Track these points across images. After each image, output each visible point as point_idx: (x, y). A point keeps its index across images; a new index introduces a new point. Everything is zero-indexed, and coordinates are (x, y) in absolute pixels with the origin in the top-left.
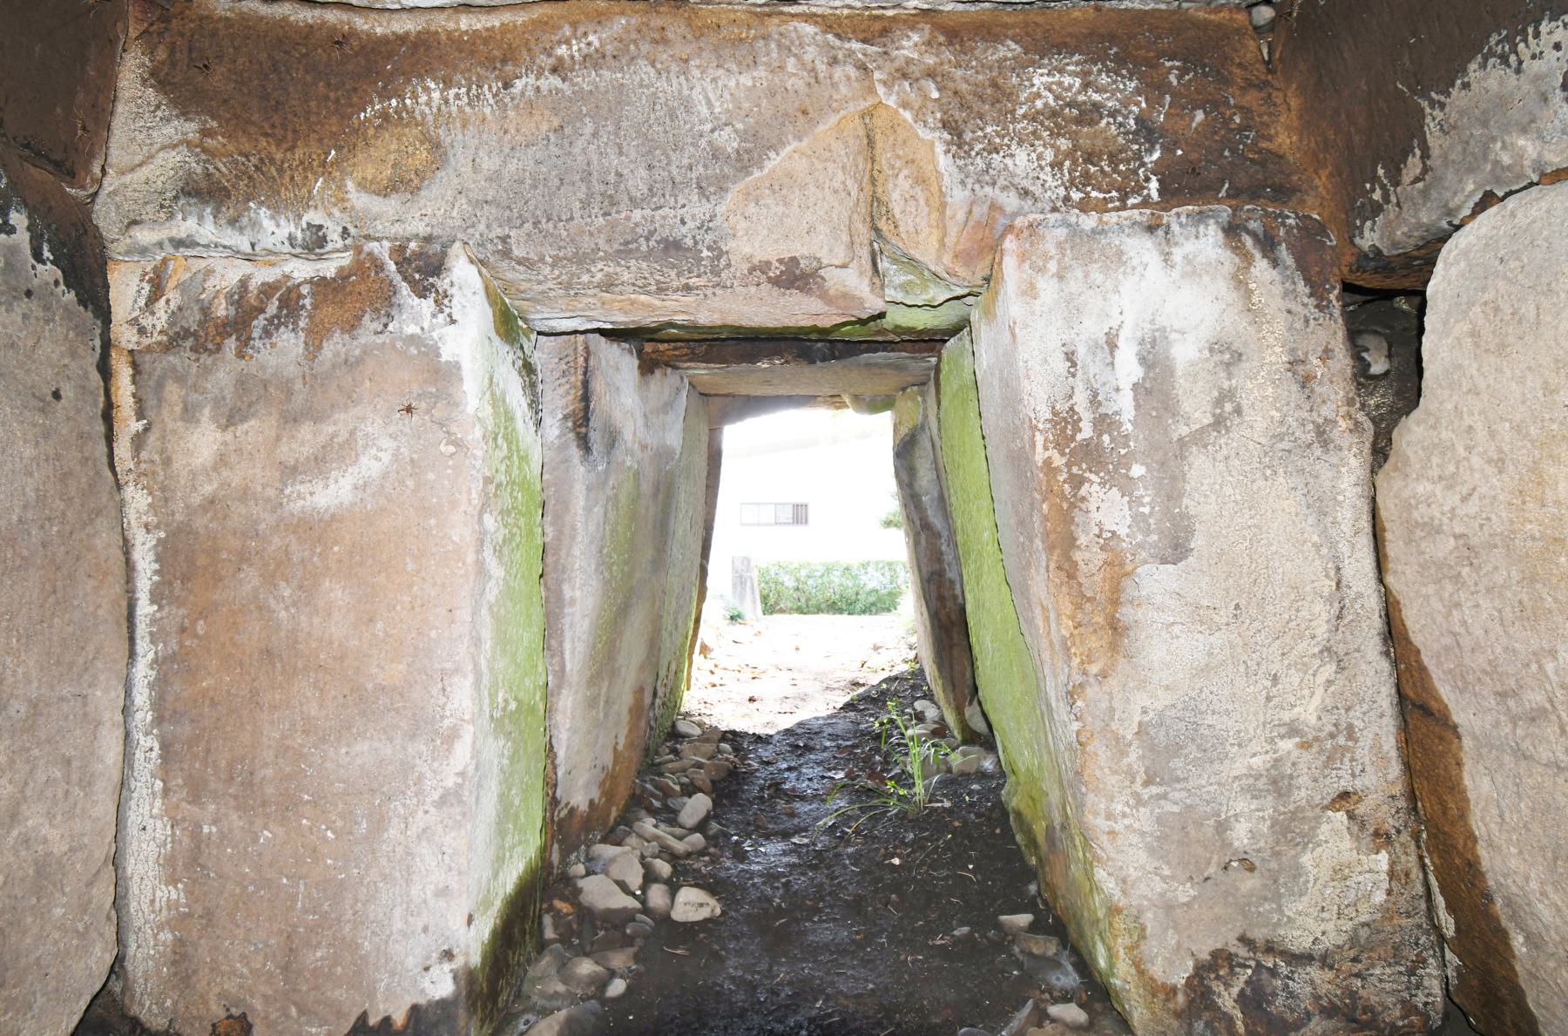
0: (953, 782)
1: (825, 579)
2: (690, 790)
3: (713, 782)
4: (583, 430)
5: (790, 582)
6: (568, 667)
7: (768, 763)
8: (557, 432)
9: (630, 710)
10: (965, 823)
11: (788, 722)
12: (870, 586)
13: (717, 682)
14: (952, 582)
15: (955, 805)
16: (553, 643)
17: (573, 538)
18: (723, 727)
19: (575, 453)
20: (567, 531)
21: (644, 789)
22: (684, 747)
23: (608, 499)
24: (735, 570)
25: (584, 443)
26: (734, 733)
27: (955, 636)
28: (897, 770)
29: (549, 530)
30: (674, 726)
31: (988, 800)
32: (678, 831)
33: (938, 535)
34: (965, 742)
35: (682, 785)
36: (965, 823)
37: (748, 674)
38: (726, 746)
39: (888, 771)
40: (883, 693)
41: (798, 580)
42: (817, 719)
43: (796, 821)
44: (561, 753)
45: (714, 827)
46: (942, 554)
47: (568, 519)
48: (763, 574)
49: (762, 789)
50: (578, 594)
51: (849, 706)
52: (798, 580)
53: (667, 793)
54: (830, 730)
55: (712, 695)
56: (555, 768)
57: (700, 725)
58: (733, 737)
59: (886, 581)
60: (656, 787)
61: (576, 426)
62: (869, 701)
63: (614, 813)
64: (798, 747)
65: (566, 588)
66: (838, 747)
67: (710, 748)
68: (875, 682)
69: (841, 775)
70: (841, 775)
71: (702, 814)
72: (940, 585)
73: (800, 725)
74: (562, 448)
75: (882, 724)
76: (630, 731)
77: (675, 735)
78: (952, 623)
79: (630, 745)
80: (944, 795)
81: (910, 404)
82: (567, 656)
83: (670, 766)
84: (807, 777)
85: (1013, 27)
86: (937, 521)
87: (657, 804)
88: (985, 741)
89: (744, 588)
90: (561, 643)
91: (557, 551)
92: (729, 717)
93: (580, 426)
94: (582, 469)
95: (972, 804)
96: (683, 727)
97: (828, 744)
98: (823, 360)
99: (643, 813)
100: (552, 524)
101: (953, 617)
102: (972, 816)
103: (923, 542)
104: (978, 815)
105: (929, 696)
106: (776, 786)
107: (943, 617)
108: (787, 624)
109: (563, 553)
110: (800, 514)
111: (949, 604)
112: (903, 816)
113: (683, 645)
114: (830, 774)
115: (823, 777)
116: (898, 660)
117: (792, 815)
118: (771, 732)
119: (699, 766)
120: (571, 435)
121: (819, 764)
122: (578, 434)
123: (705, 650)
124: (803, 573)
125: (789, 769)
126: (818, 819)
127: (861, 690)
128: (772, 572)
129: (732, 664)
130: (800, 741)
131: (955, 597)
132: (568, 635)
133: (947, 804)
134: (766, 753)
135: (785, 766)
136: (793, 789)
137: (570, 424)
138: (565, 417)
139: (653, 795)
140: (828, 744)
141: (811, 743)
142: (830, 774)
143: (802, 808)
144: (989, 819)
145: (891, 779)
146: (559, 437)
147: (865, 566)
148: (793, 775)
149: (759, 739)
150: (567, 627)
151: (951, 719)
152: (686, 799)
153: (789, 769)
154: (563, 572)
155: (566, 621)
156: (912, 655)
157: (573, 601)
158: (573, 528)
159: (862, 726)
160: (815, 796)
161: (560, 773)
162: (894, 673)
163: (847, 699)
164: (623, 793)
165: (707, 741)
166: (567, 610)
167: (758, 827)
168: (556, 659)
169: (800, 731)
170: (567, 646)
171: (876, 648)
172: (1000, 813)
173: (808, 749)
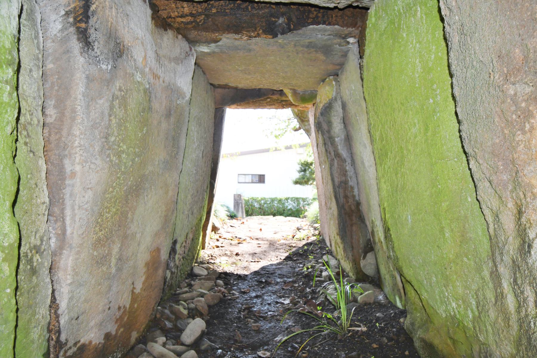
0: (363, 311)
1: (271, 204)
2: (194, 313)
3: (209, 306)
4: (83, 25)
5: (256, 205)
6: (69, 231)
7: (244, 293)
8: (60, 27)
9: (147, 264)
10: (381, 345)
11: (255, 267)
12: (289, 208)
13: (220, 245)
14: (352, 188)
15: (369, 330)
16: (56, 210)
17: (73, 119)
18: (220, 270)
19: (75, 45)
20: (67, 114)
21: (162, 313)
22: (196, 283)
23: (114, 97)
24: (235, 200)
25: (84, 37)
26: (226, 274)
27: (354, 218)
28: (321, 299)
29: (51, 111)
30: (192, 269)
31: (393, 327)
32: (179, 348)
33: (344, 161)
34: (358, 280)
35: (189, 309)
36: (381, 345)
37: (236, 242)
38: (220, 282)
39: (316, 299)
40: (305, 251)
41: (260, 205)
42: (272, 265)
43: (261, 336)
44: (63, 304)
45: (206, 343)
46: (346, 171)
47: (68, 103)
48: (247, 202)
49: (240, 312)
50: (78, 168)
51: (288, 258)
52: (260, 205)
53: (178, 316)
54: (279, 272)
55: (217, 252)
56: (57, 317)
57: (208, 269)
58: (226, 276)
59: (295, 205)
60: (172, 312)
61: (77, 21)
62: (298, 255)
63: (135, 335)
64: (262, 282)
65: (67, 162)
66: (285, 282)
67: (210, 284)
68: (301, 246)
69: (287, 301)
70: (287, 301)
71: (198, 333)
72: (345, 189)
73: (263, 268)
74: (64, 40)
75: (308, 268)
76: (147, 279)
77: (192, 275)
78: (352, 211)
79: (147, 286)
80: (361, 321)
81: (327, 88)
82: (68, 221)
83: (184, 296)
84: (268, 303)
85: (329, 30)
86: (344, 153)
87: (169, 325)
88: (376, 282)
89: (238, 207)
90: (63, 210)
91: (59, 131)
92: (224, 265)
93: (80, 21)
94: (82, 60)
95: (382, 330)
96: (197, 270)
97: (279, 280)
98: (282, 34)
99: (158, 332)
100: (55, 107)
101: (353, 208)
102: (385, 340)
103: (336, 164)
104: (390, 339)
105: (330, 253)
106: (249, 309)
107: (346, 207)
108: (255, 221)
109: (64, 132)
110: (261, 179)
111: (351, 200)
112: (333, 336)
113: (198, 225)
114: (281, 300)
115: (277, 303)
116: (310, 235)
117: (258, 331)
118: (246, 273)
119: (202, 295)
120: (72, 29)
121: (274, 293)
122: (78, 28)
123: (215, 229)
124: (262, 202)
125: (257, 297)
126: (275, 335)
127: (294, 249)
128: (250, 201)
129: (228, 236)
130: (263, 278)
131: (354, 196)
132: (68, 203)
133: (365, 329)
134: (243, 286)
135: (254, 294)
136: (259, 312)
137: (71, 20)
138: (67, 14)
139: (168, 319)
140: (279, 280)
141: (269, 280)
142: (281, 300)
143: (265, 325)
144: (397, 342)
145: (319, 305)
146: (62, 30)
147: (287, 199)
148: (259, 301)
149: (239, 277)
150: (67, 197)
151: (347, 266)
152: (191, 320)
153: (257, 297)
154: (64, 149)
155: (67, 191)
156: (317, 232)
157: (73, 174)
158: (74, 111)
159: (297, 270)
160: (273, 316)
161: (62, 321)
162: (309, 241)
163: (287, 254)
164: (143, 321)
165: (209, 279)
166: (67, 182)
167: (236, 341)
168: (59, 224)
169: (263, 272)
170: (68, 212)
171: (298, 229)
172: (405, 338)
173: (267, 283)
